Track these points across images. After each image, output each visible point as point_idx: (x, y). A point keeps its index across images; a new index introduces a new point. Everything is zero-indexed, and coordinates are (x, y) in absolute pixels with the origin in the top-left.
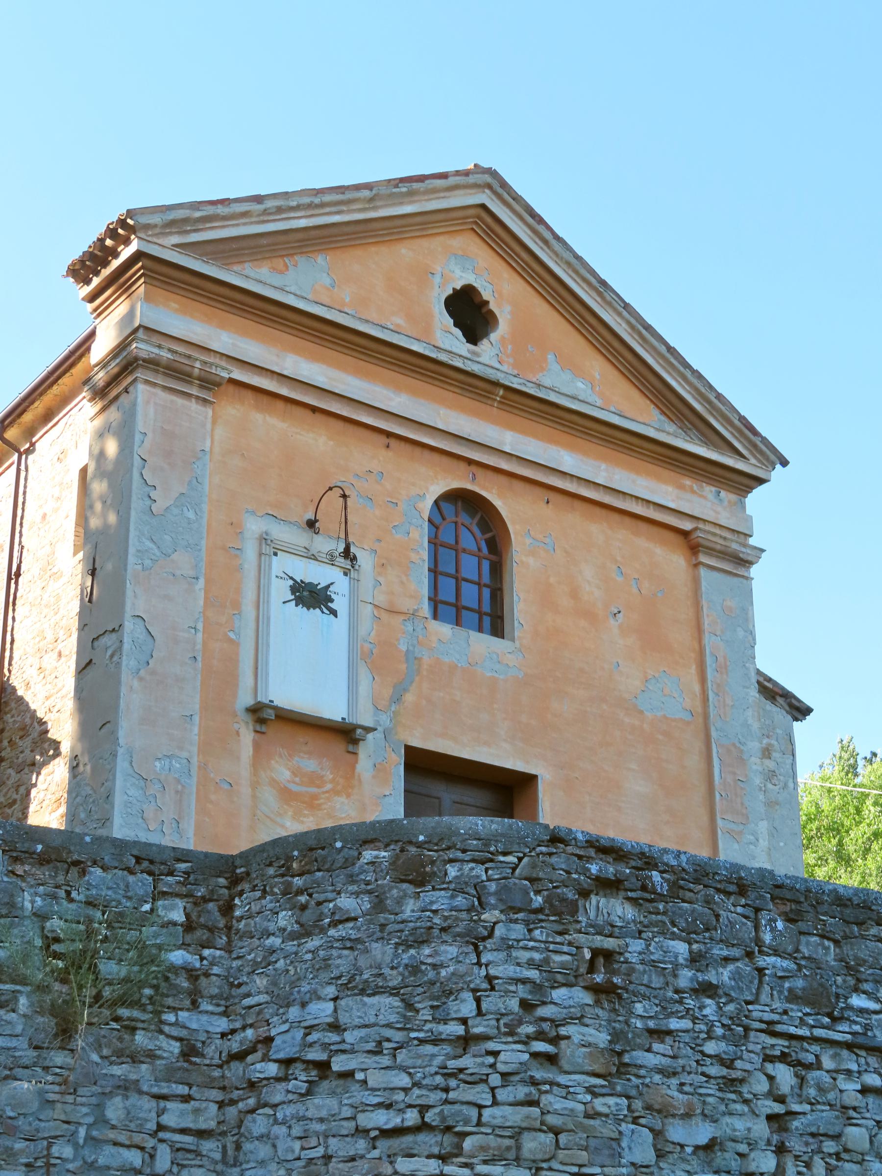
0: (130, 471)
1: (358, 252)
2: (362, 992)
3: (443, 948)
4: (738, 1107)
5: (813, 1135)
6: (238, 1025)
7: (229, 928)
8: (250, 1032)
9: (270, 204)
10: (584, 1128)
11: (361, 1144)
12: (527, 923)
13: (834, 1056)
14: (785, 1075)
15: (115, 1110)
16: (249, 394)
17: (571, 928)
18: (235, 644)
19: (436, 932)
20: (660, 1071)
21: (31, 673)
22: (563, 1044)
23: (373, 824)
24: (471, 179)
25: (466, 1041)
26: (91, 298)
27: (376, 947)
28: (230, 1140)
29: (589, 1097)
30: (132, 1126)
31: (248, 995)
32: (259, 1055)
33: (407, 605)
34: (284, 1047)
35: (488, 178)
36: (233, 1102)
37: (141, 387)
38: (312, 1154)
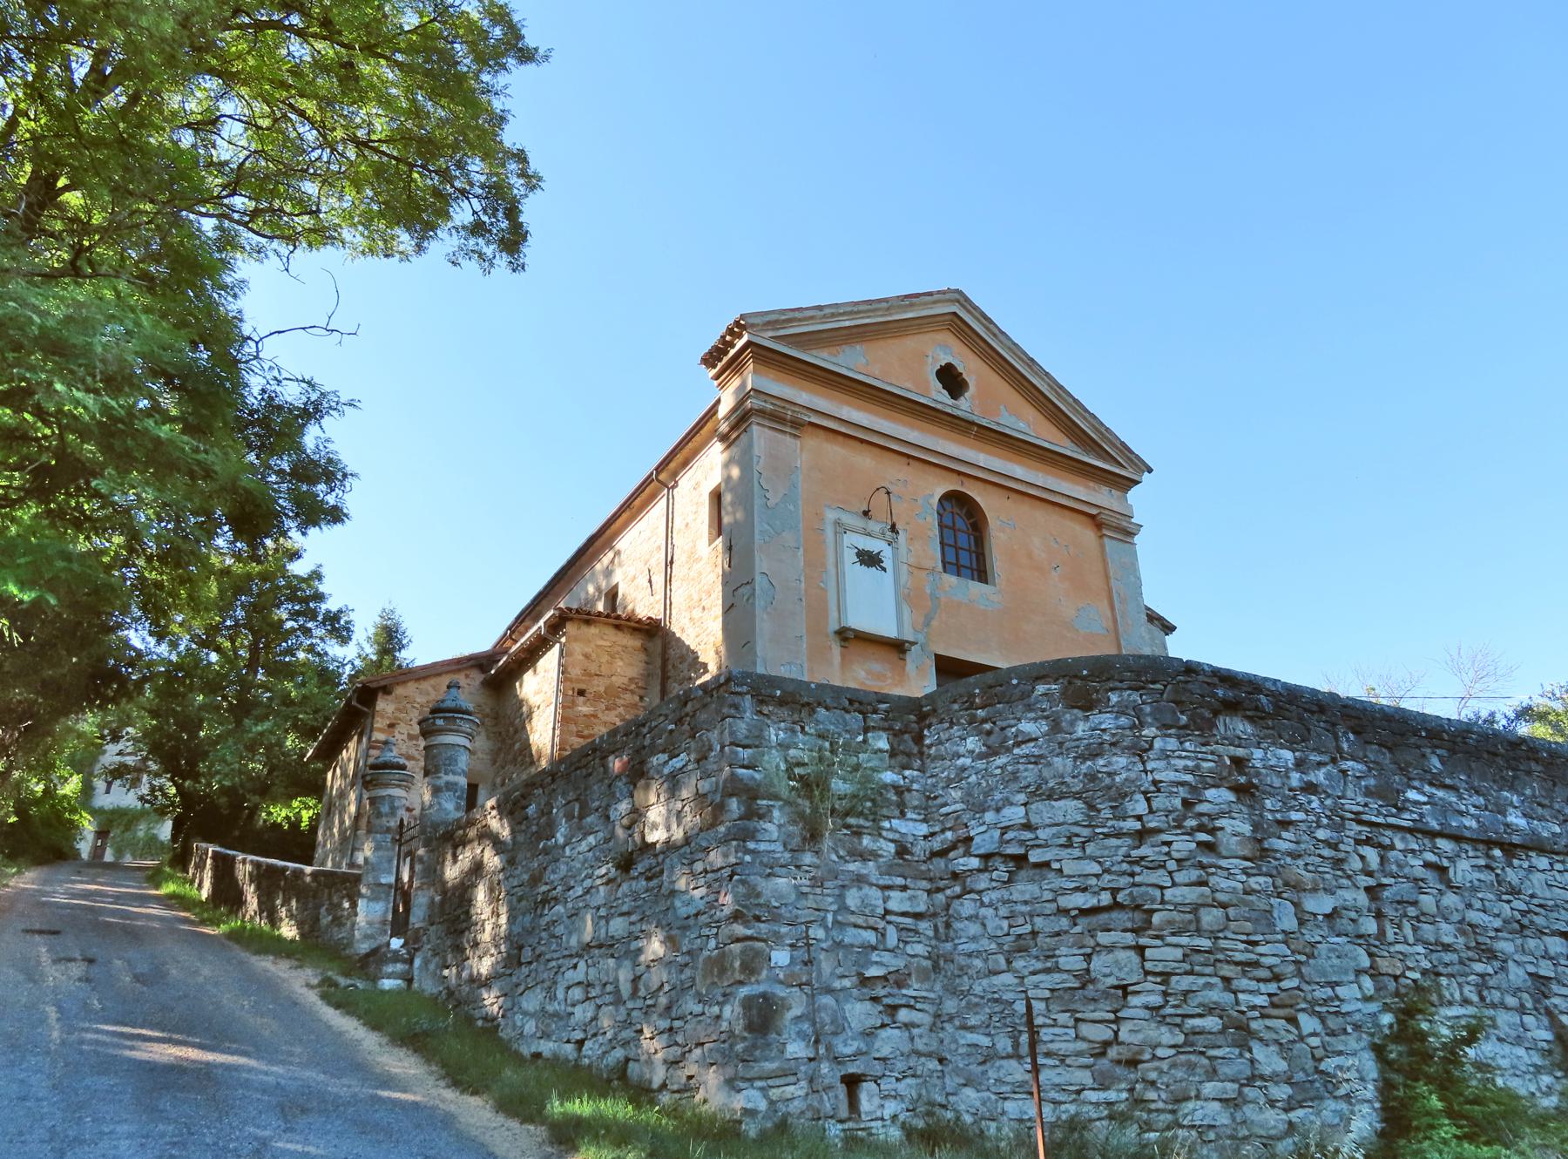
0: (751, 480)
1: (881, 343)
2: (1050, 797)
3: (1115, 759)
4: (1345, 882)
5: (1399, 902)
6: (937, 829)
7: (921, 753)
8: (949, 834)
9: (827, 311)
10: (1246, 904)
11: (1064, 922)
12: (1178, 737)
13: (1403, 839)
14: (1372, 855)
15: (853, 898)
16: (821, 432)
17: (1213, 739)
18: (824, 590)
19: (1106, 746)
20: (1290, 854)
21: (685, 622)
22: (1219, 834)
23: (1042, 664)
24: (947, 296)
25: (1142, 835)
26: (717, 377)
27: (1058, 761)
28: (940, 922)
29: (1244, 878)
30: (867, 911)
31: (945, 805)
32: (961, 850)
33: (928, 564)
34: (985, 841)
35: (957, 296)
36: (939, 890)
37: (755, 428)
38: (1020, 931)
